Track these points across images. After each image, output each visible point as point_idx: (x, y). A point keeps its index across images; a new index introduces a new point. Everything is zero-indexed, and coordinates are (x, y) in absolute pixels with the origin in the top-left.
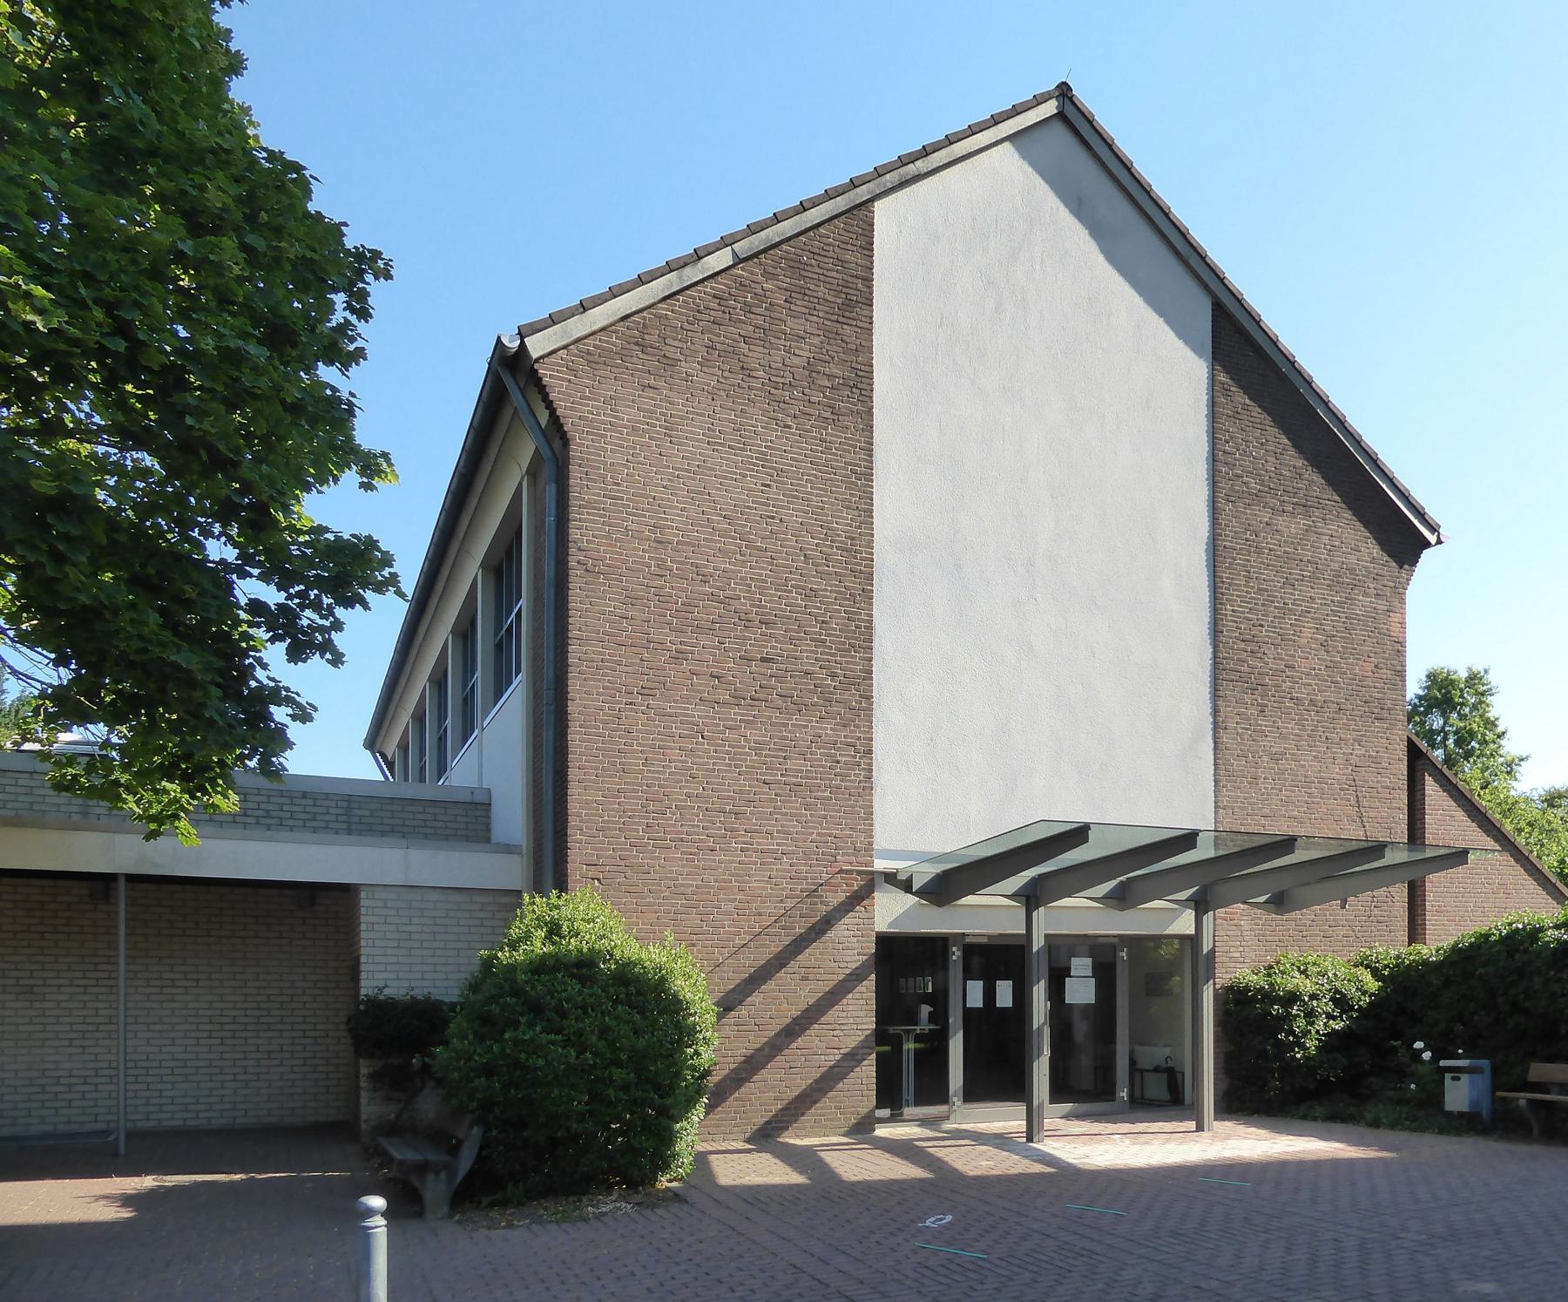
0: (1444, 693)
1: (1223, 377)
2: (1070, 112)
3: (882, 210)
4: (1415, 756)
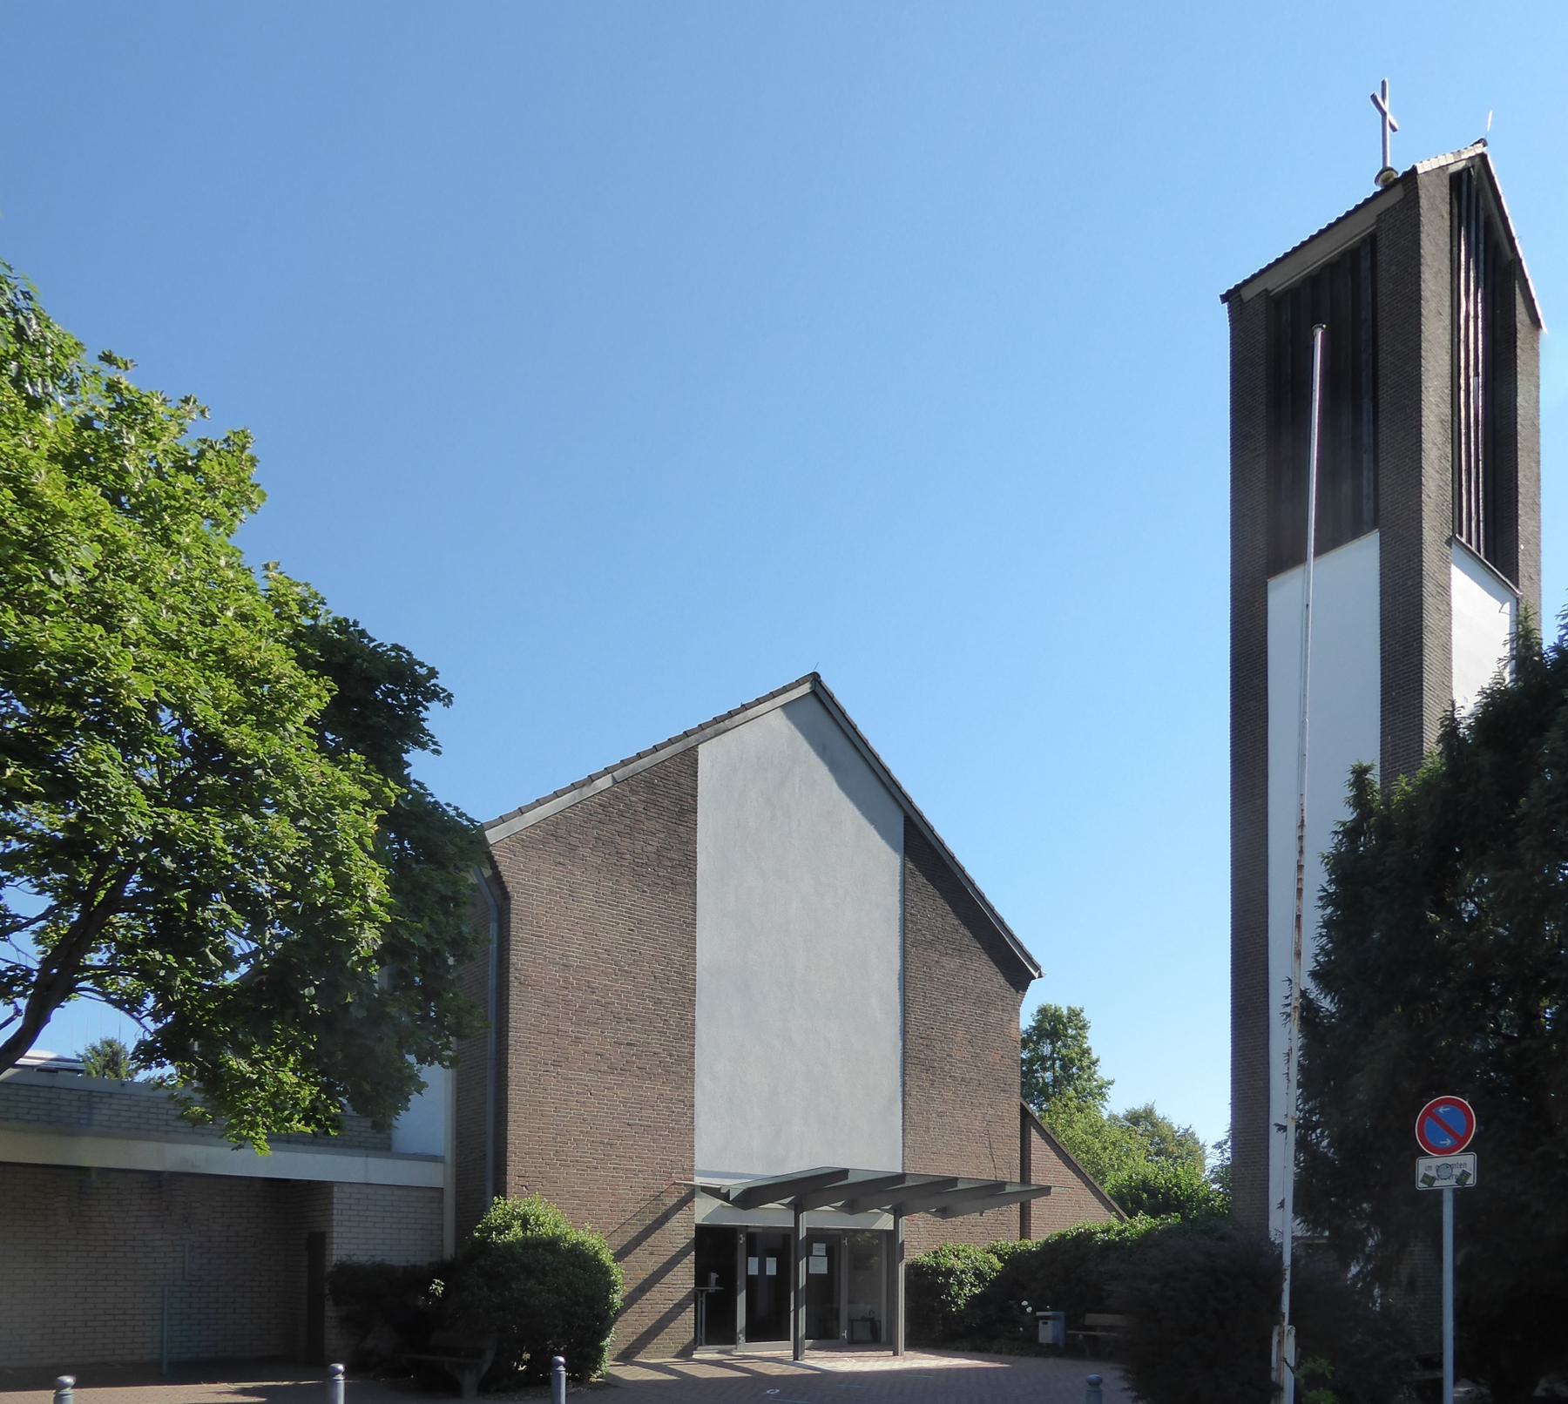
0: (1054, 1026)
1: (910, 865)
2: (819, 690)
3: (703, 750)
4: (1025, 1113)
